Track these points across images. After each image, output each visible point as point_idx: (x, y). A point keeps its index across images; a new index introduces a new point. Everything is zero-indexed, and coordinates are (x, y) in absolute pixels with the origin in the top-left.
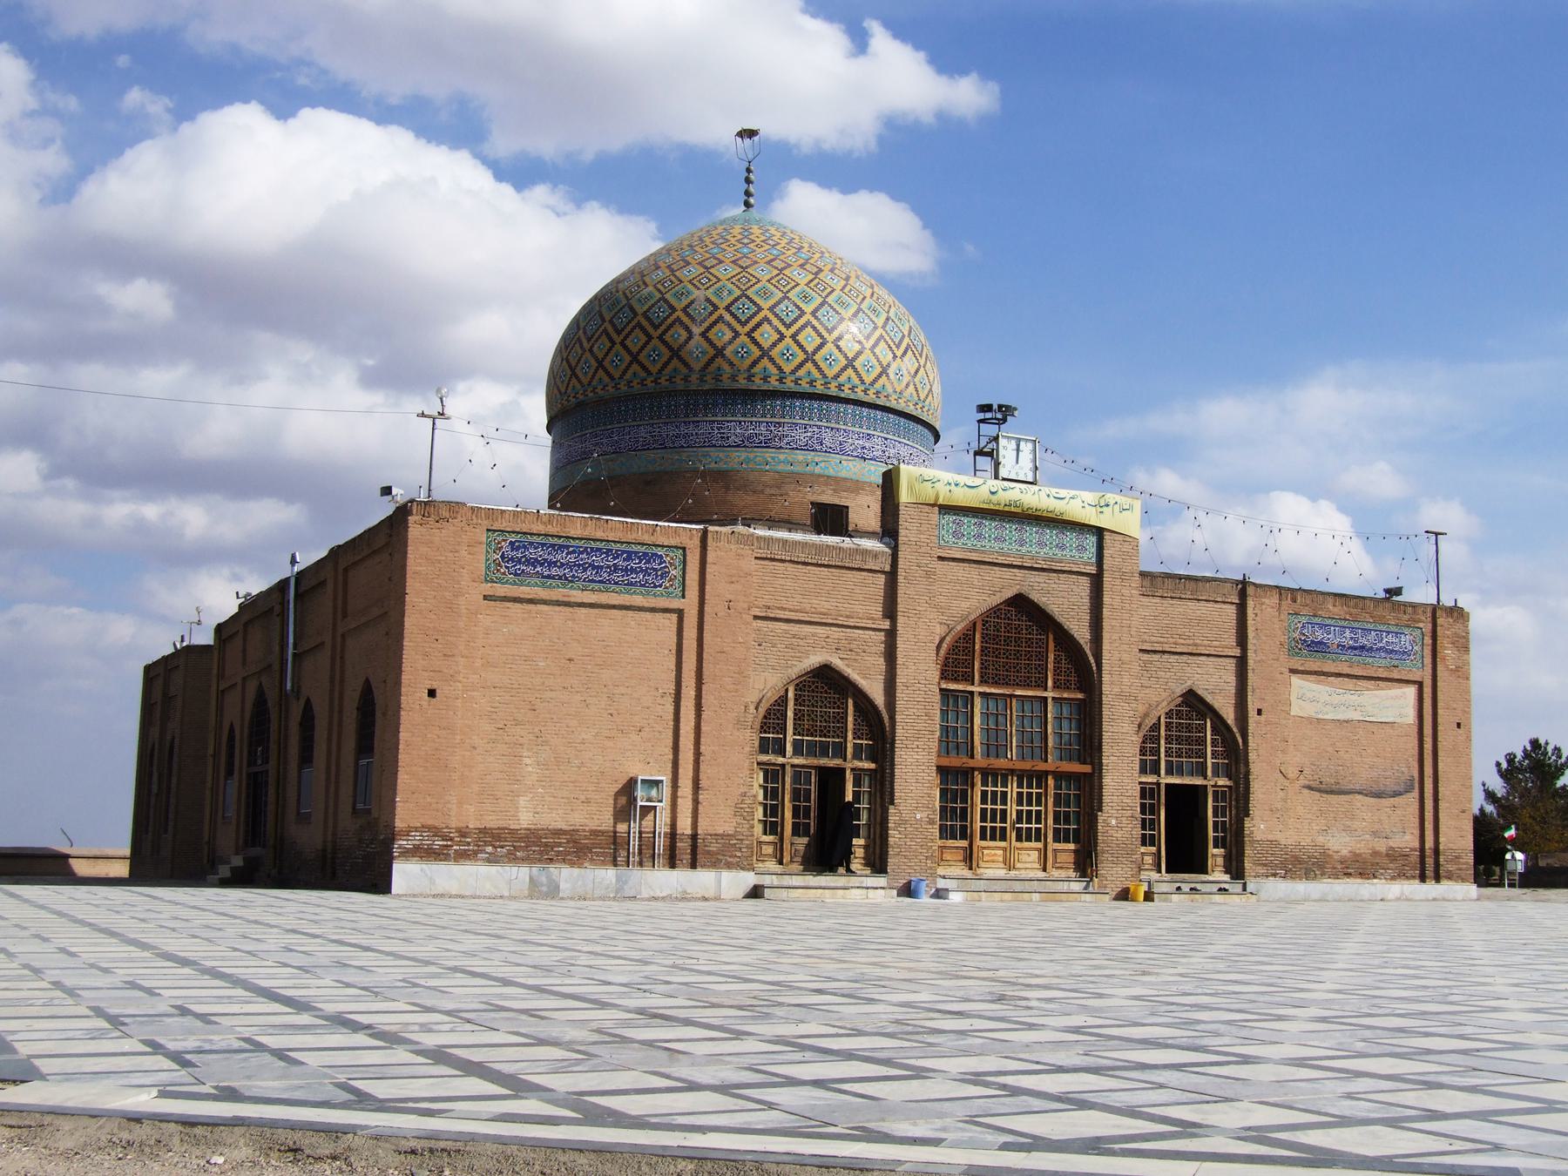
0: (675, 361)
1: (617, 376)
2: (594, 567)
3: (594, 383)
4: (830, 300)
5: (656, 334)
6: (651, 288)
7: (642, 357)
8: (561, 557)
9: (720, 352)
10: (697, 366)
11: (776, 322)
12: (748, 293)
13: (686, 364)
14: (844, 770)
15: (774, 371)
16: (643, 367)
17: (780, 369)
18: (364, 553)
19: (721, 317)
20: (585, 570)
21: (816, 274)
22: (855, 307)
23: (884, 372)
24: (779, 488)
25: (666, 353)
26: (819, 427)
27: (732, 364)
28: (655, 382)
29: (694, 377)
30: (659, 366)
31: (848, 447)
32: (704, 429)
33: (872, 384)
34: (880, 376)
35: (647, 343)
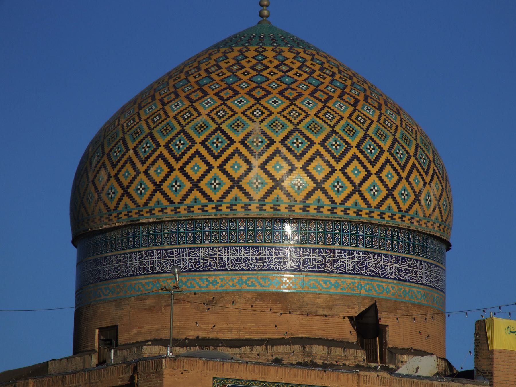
0: (236, 191)
1: (176, 200)
3: (151, 204)
4: (370, 132)
5: (162, 149)
6: (204, 117)
7: (203, 185)
9: (277, 184)
10: (257, 196)
11: (327, 156)
12: (300, 126)
13: (246, 194)
15: (327, 202)
17: (331, 200)
19: (277, 151)
21: (315, 91)
22: (361, 134)
23: (417, 199)
24: (330, 308)
25: (227, 183)
26: (364, 253)
27: (288, 195)
28: (216, 208)
29: (254, 207)
30: (219, 194)
32: (263, 254)
33: (407, 211)
34: (413, 203)
35: (207, 172)
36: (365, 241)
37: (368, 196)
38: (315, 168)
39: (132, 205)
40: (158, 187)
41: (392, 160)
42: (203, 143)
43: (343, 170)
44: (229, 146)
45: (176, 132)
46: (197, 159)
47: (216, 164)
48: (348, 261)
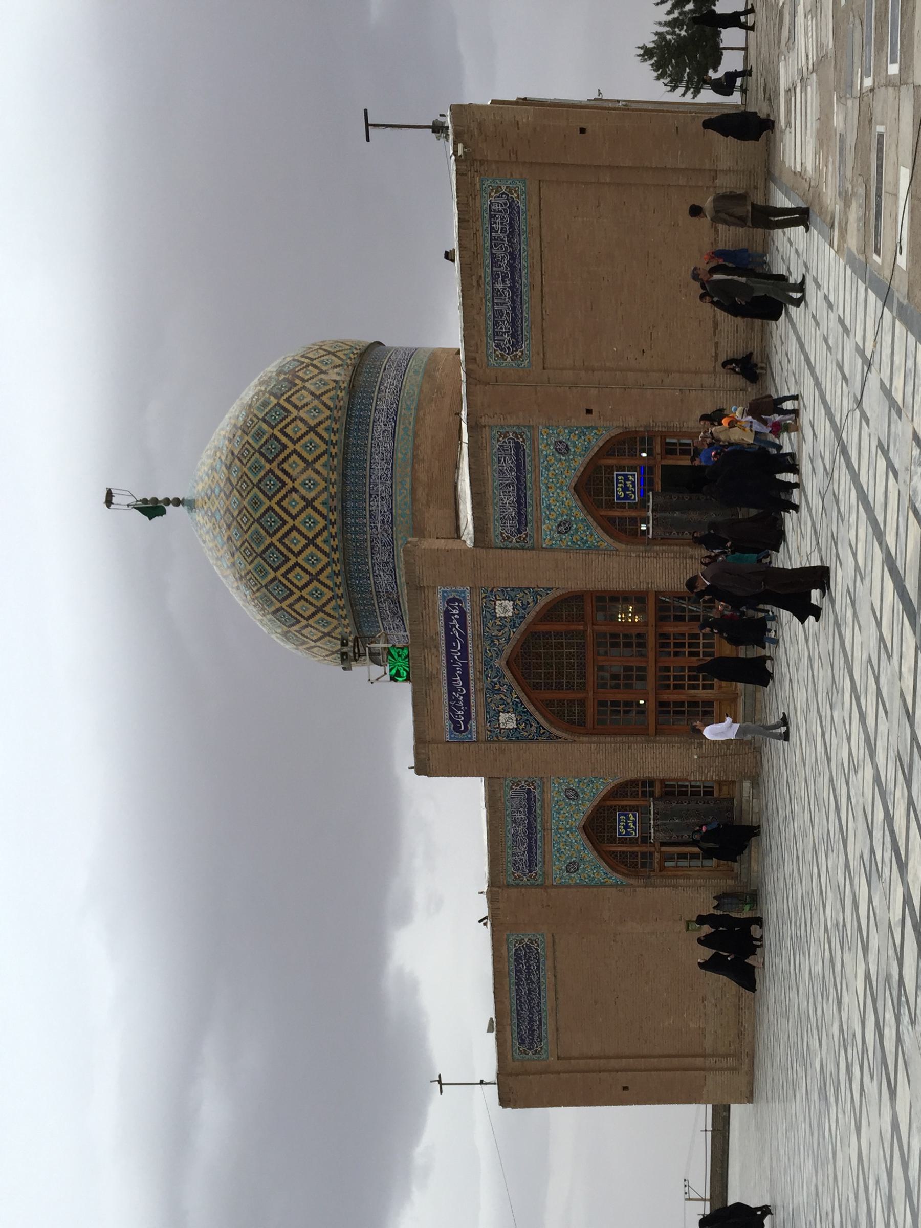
2: (530, 993)
8: (525, 1013)
12: (255, 482)
14: (664, 467)
16: (319, 533)
18: (519, 300)
20: (533, 999)
31: (386, 539)
36: (361, 533)
37: (319, 567)
38: (296, 432)
39: (328, 571)
40: (311, 542)
41: (281, 426)
42: (270, 499)
43: (294, 518)
44: (273, 510)
45: (262, 562)
46: (286, 541)
47: (291, 522)
48: (384, 579)
